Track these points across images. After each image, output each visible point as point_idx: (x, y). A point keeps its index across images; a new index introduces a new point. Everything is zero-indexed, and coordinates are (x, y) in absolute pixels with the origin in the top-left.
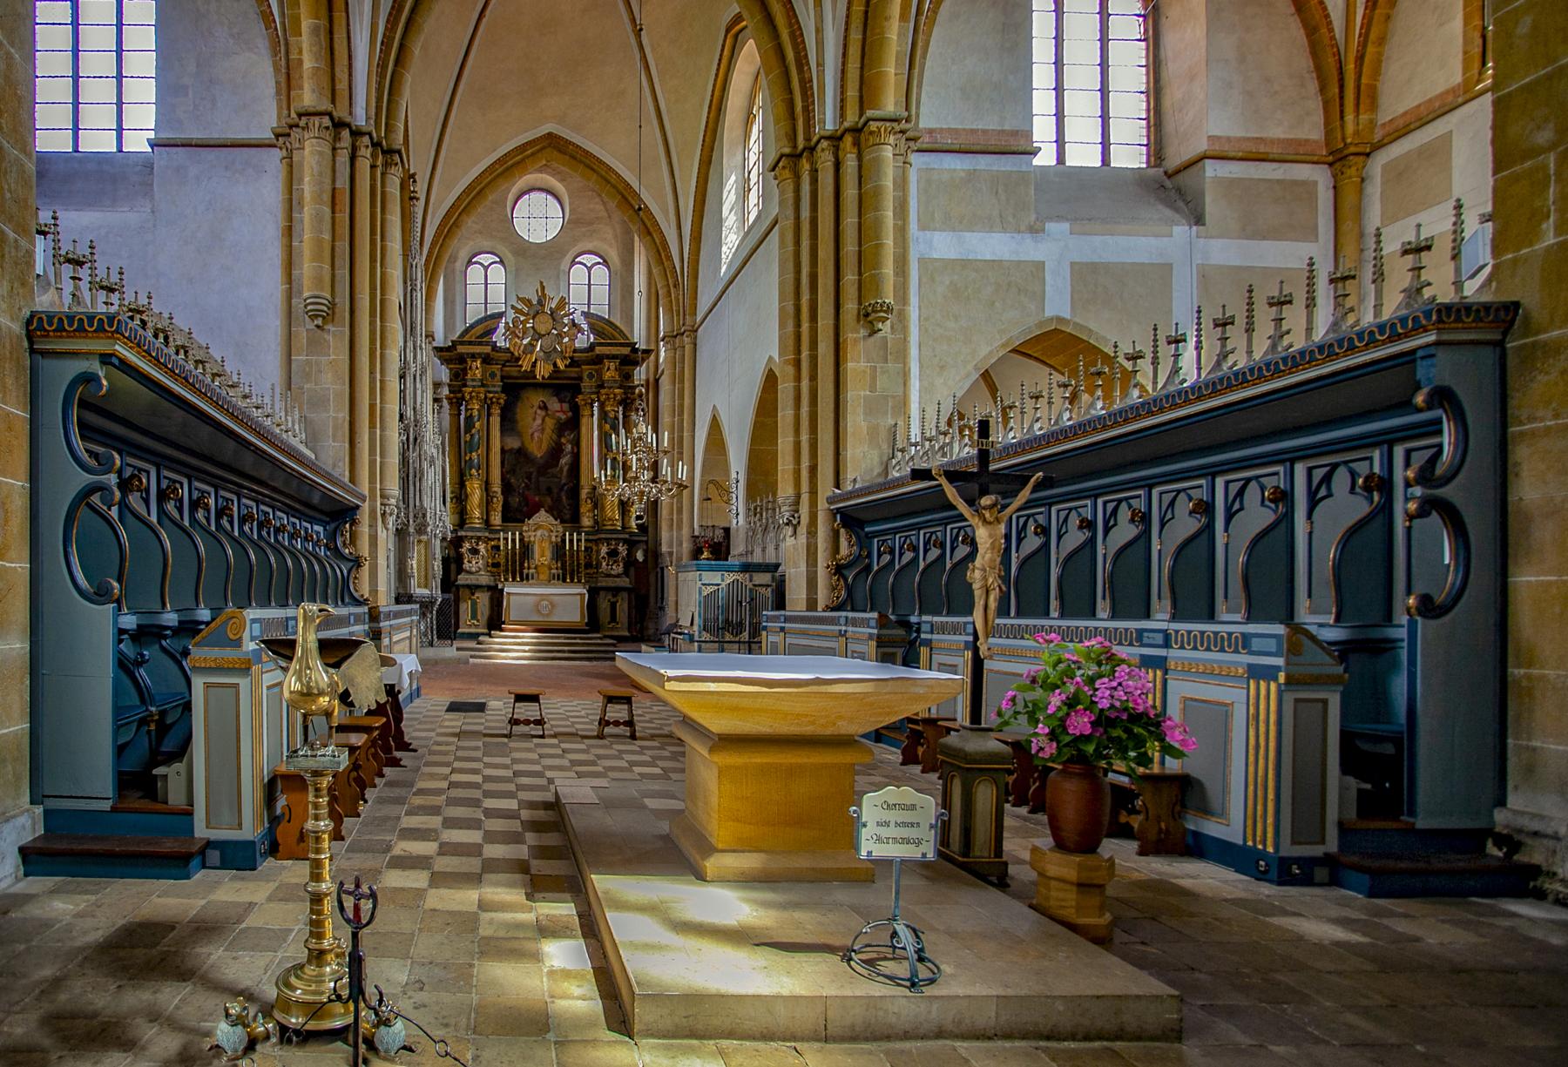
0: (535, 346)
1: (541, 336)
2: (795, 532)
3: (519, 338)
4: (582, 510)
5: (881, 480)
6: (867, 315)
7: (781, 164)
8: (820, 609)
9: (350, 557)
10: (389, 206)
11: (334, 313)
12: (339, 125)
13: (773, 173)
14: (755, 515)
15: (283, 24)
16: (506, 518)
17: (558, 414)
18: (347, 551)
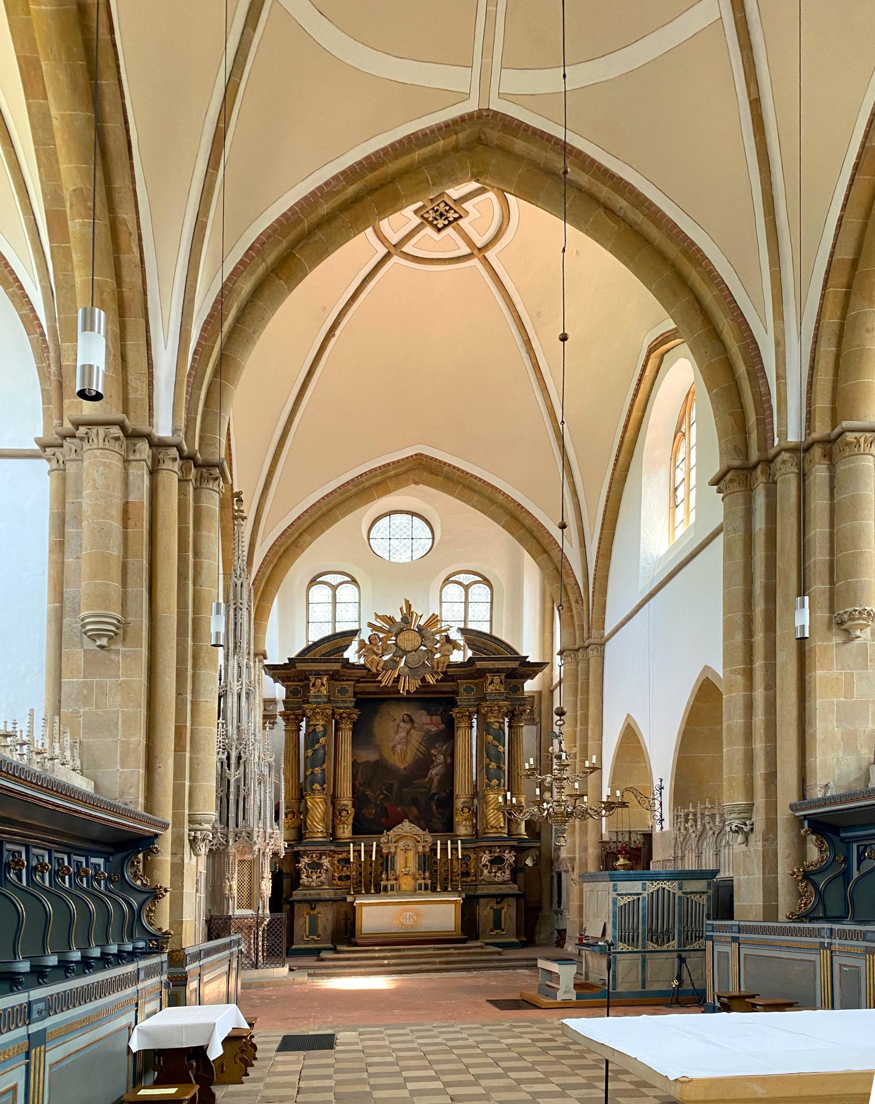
0: (398, 663)
1: (406, 653)
2: (747, 839)
3: (377, 655)
4: (456, 819)
5: (860, 787)
6: (842, 623)
7: (728, 477)
8: (782, 917)
9: (143, 889)
10: (205, 522)
11: (125, 633)
12: (132, 436)
13: (716, 487)
14: (687, 821)
15: (52, 329)
16: (358, 829)
17: (426, 727)
18: (139, 883)
